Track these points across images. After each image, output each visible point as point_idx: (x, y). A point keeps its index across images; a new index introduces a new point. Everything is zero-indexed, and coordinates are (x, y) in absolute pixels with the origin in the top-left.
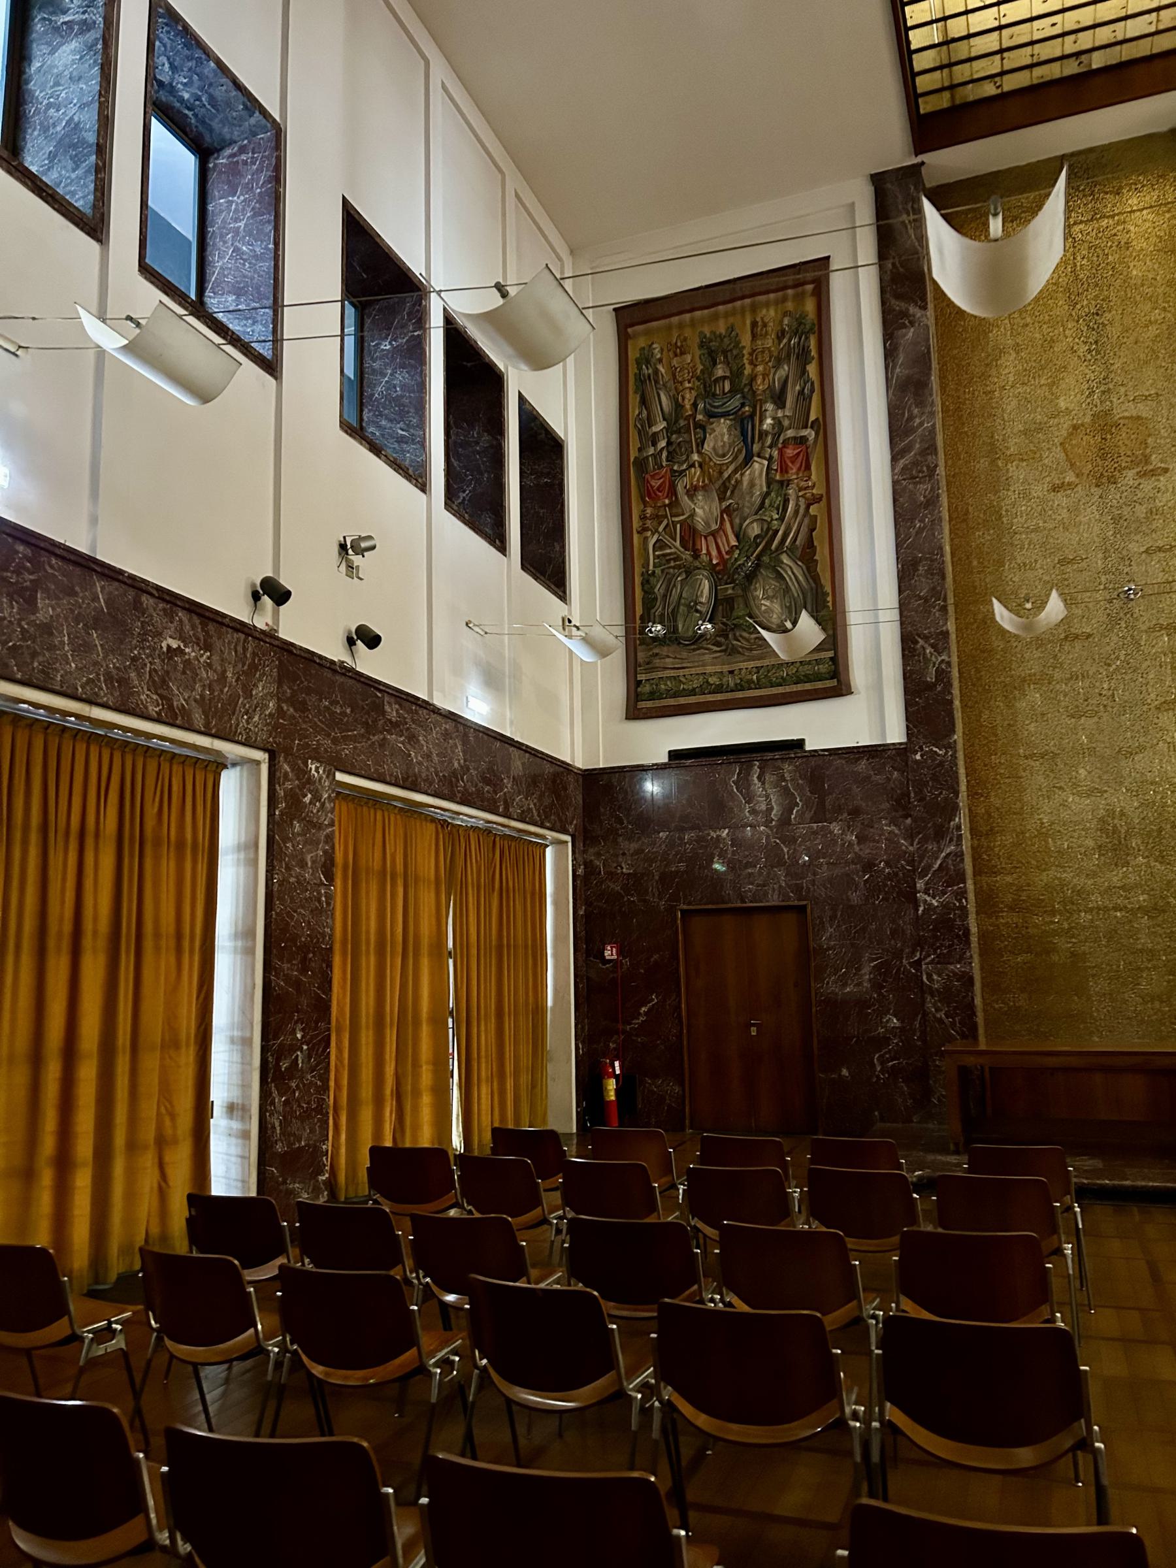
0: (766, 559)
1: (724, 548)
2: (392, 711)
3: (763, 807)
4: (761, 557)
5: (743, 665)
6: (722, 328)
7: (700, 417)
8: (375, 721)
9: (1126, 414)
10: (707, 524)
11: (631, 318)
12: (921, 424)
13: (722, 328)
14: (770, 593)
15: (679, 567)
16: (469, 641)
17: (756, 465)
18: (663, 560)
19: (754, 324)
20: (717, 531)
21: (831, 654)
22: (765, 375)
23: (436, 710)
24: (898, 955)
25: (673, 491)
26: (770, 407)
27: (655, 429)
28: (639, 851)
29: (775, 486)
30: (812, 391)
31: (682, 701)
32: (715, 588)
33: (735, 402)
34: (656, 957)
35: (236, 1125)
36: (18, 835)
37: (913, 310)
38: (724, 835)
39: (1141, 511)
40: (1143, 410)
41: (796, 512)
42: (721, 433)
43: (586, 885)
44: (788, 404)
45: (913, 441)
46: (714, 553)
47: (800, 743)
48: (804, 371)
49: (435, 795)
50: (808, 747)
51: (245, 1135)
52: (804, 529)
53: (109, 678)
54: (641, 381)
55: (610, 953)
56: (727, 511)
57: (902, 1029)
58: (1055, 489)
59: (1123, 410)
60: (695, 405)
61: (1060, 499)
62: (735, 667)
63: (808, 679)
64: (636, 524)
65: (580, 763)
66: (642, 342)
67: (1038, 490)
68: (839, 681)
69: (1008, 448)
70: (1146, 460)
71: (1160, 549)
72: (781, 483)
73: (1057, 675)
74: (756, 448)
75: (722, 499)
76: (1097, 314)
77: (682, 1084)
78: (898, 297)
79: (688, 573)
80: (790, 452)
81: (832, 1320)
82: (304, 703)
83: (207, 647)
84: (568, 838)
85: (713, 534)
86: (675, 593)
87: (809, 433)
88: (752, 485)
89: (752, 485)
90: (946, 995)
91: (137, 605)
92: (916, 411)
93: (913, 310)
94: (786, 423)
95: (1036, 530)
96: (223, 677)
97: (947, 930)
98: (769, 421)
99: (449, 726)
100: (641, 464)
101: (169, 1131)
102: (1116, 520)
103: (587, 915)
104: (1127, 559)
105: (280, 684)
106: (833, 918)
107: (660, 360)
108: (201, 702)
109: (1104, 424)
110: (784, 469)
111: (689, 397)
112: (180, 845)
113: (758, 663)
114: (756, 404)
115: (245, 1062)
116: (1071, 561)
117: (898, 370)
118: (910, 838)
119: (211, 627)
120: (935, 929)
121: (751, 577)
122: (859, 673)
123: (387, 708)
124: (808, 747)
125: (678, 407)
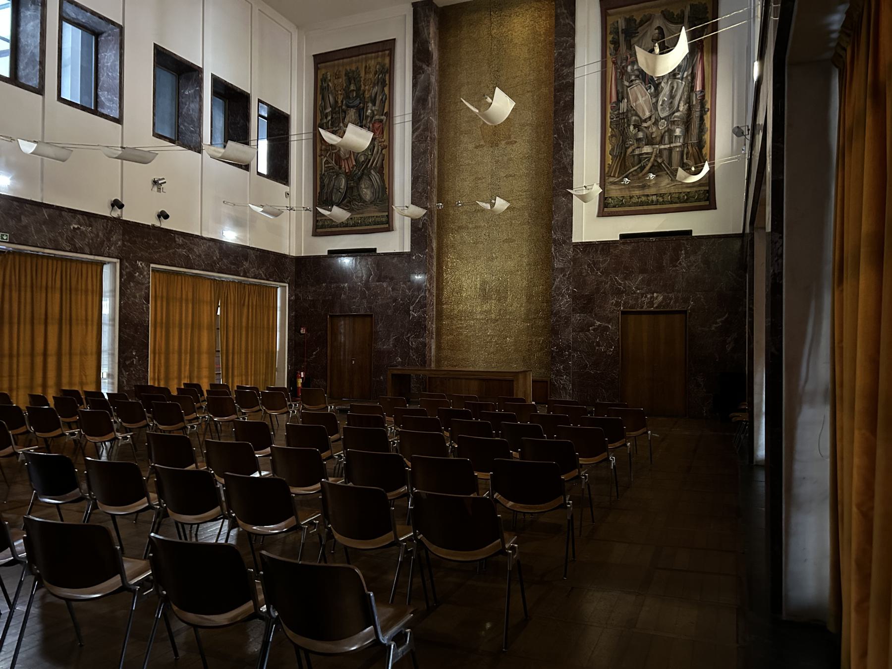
1: (351, 166)
2: (180, 241)
6: (354, 68)
11: (320, 60)
16: (226, 210)
18: (329, 169)
22: (369, 91)
26: (370, 105)
28: (315, 291)
31: (333, 229)
32: (347, 182)
33: (357, 102)
35: (110, 380)
36: (23, 289)
37: (424, 66)
39: (506, 158)
48: (383, 90)
49: (203, 270)
51: (113, 384)
53: (50, 240)
54: (322, 89)
55: (303, 331)
58: (476, 147)
65: (293, 254)
66: (323, 71)
67: (471, 146)
70: (510, 138)
71: (511, 176)
73: (470, 226)
78: (419, 60)
79: (337, 175)
81: (324, 455)
83: (91, 226)
85: (347, 159)
91: (61, 216)
93: (424, 66)
95: (469, 164)
96: (97, 236)
97: (419, 326)
99: (211, 244)
101: (84, 381)
102: (497, 162)
103: (296, 316)
105: (123, 235)
108: (88, 245)
111: (340, 98)
112: (87, 291)
114: (365, 103)
115: (113, 361)
116: (480, 179)
119: (92, 219)
121: (360, 179)
122: (397, 222)
125: (336, 102)
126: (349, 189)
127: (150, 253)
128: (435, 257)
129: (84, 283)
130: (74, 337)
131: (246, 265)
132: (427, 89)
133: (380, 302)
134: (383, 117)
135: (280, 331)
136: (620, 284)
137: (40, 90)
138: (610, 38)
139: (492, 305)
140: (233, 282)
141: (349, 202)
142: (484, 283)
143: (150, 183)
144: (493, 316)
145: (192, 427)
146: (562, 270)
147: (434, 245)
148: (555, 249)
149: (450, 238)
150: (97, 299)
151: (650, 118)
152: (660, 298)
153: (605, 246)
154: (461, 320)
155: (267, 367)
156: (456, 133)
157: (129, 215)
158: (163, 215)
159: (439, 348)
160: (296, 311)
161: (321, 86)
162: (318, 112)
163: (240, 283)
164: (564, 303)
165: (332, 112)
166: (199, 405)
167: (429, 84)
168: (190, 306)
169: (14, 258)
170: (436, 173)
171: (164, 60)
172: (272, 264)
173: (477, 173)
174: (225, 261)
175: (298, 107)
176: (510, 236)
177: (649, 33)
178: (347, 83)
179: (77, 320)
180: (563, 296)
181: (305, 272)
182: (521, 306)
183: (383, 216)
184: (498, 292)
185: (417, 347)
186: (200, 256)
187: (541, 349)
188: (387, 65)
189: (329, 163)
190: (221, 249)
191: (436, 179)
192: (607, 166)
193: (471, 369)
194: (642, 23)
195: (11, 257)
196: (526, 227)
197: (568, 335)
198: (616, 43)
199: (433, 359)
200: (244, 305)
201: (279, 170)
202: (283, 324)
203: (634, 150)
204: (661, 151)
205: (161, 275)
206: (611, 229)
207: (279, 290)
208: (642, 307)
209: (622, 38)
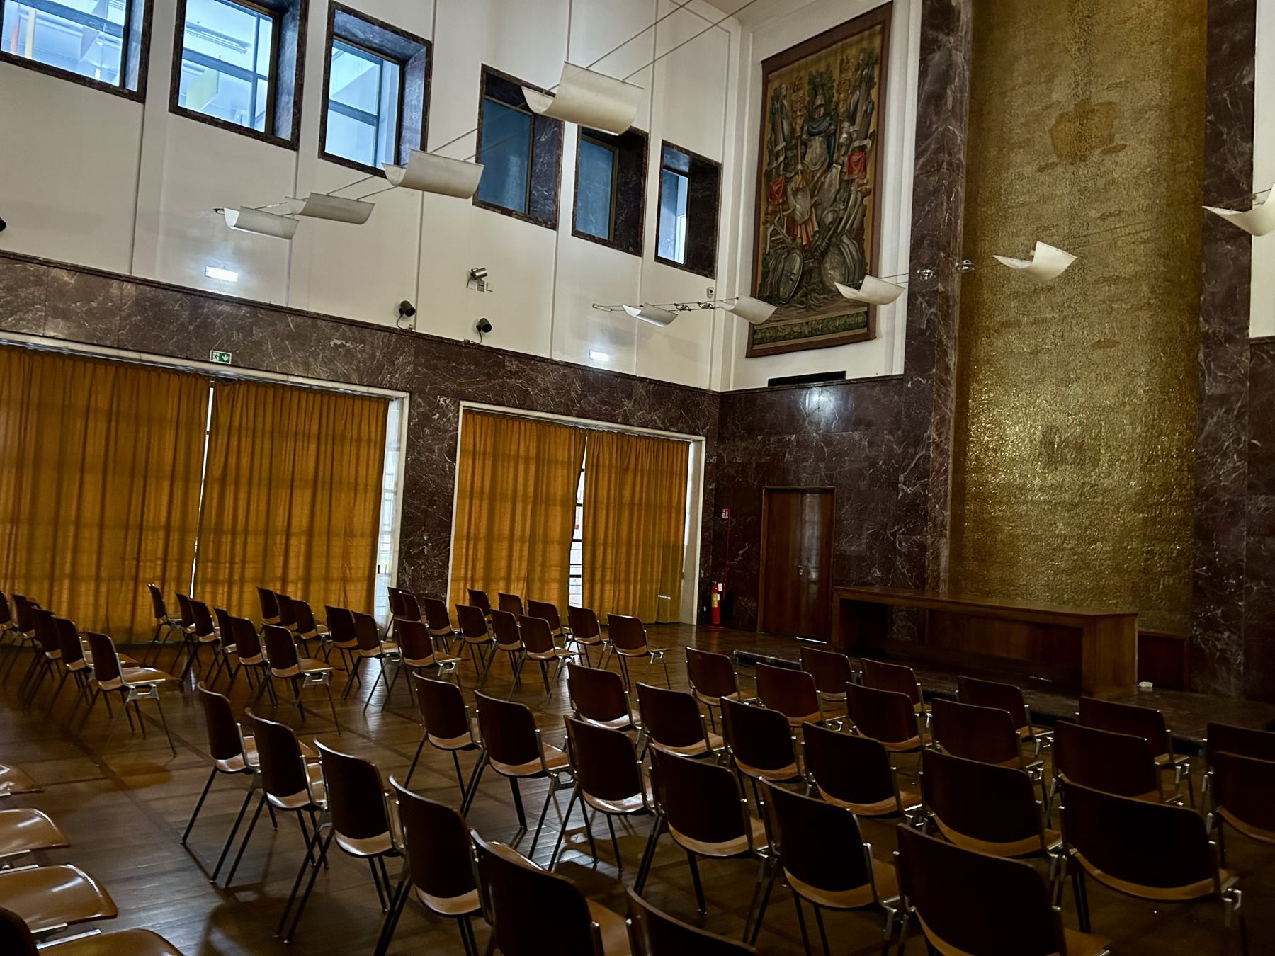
0: (834, 240)
1: (811, 233)
4: (830, 237)
5: (814, 318)
6: (822, 68)
8: (496, 372)
13: (822, 68)
15: (783, 248)
16: (596, 318)
19: (842, 61)
23: (556, 363)
24: (884, 526)
25: (785, 193)
26: (846, 124)
27: (779, 148)
28: (746, 448)
29: (844, 185)
32: (803, 261)
33: (826, 124)
37: (942, 37)
40: (1113, 96)
42: (817, 146)
43: (713, 472)
46: (804, 236)
47: (842, 374)
48: (869, 94)
50: (848, 377)
52: (859, 215)
54: (773, 113)
55: (725, 515)
56: (814, 205)
57: (882, 578)
58: (1041, 169)
59: (1101, 96)
61: (1044, 178)
62: (809, 319)
63: (851, 327)
65: (717, 388)
66: (776, 84)
67: (1029, 170)
70: (1111, 140)
71: (1111, 215)
74: (835, 156)
75: (812, 197)
77: (757, 602)
79: (789, 252)
80: (855, 158)
82: (435, 365)
83: (363, 342)
84: (704, 439)
85: (805, 223)
86: (780, 267)
87: (868, 142)
88: (830, 185)
89: (830, 185)
90: (909, 557)
92: (934, 119)
93: (942, 37)
94: (855, 136)
95: (1024, 204)
96: (373, 356)
97: (915, 513)
98: (844, 136)
100: (768, 175)
102: (1082, 192)
103: (717, 489)
105: (416, 356)
106: (849, 499)
109: (1084, 111)
110: (850, 172)
111: (800, 122)
112: (359, 440)
114: (836, 121)
116: (1046, 228)
118: (899, 444)
120: (908, 510)
123: (508, 364)
124: (848, 377)
125: (793, 130)
126: (806, 273)
127: (460, 385)
128: (954, 382)
129: (355, 427)
130: (333, 514)
131: (629, 405)
132: (945, 78)
133: (847, 466)
134: (868, 142)
135: (691, 513)
137: (293, 145)
139: (1066, 475)
140: (609, 432)
141: (805, 295)
142: (1049, 430)
143: (465, 278)
144: (1068, 497)
145: (658, 654)
146: (1223, 400)
147: (953, 360)
148: (1207, 355)
149: (984, 347)
150: (373, 454)
154: (1000, 502)
155: (664, 571)
156: (1000, 150)
157: (424, 325)
158: (407, 310)
159: (956, 555)
160: (718, 482)
161: (772, 108)
162: (766, 150)
163: (621, 434)
164: (1229, 470)
165: (786, 149)
166: (558, 632)
167: (951, 65)
168: (532, 468)
169: (10, 357)
170: (960, 227)
171: (500, 90)
172: (678, 404)
173: (1040, 218)
174: (592, 399)
175: (733, 147)
176: (1108, 336)
178: (813, 99)
179: (341, 483)
181: (741, 421)
182: (1129, 478)
183: (858, 315)
184: (1079, 448)
185: (910, 552)
186: (546, 390)
187: (1176, 570)
188: (878, 50)
189: (778, 233)
190: (584, 380)
191: (960, 239)
193: (996, 602)
195: (243, 388)
196: (1145, 315)
197: (1239, 542)
199: (944, 575)
200: (627, 469)
201: (701, 258)
202: (695, 503)
205: (485, 420)
207: (692, 447)
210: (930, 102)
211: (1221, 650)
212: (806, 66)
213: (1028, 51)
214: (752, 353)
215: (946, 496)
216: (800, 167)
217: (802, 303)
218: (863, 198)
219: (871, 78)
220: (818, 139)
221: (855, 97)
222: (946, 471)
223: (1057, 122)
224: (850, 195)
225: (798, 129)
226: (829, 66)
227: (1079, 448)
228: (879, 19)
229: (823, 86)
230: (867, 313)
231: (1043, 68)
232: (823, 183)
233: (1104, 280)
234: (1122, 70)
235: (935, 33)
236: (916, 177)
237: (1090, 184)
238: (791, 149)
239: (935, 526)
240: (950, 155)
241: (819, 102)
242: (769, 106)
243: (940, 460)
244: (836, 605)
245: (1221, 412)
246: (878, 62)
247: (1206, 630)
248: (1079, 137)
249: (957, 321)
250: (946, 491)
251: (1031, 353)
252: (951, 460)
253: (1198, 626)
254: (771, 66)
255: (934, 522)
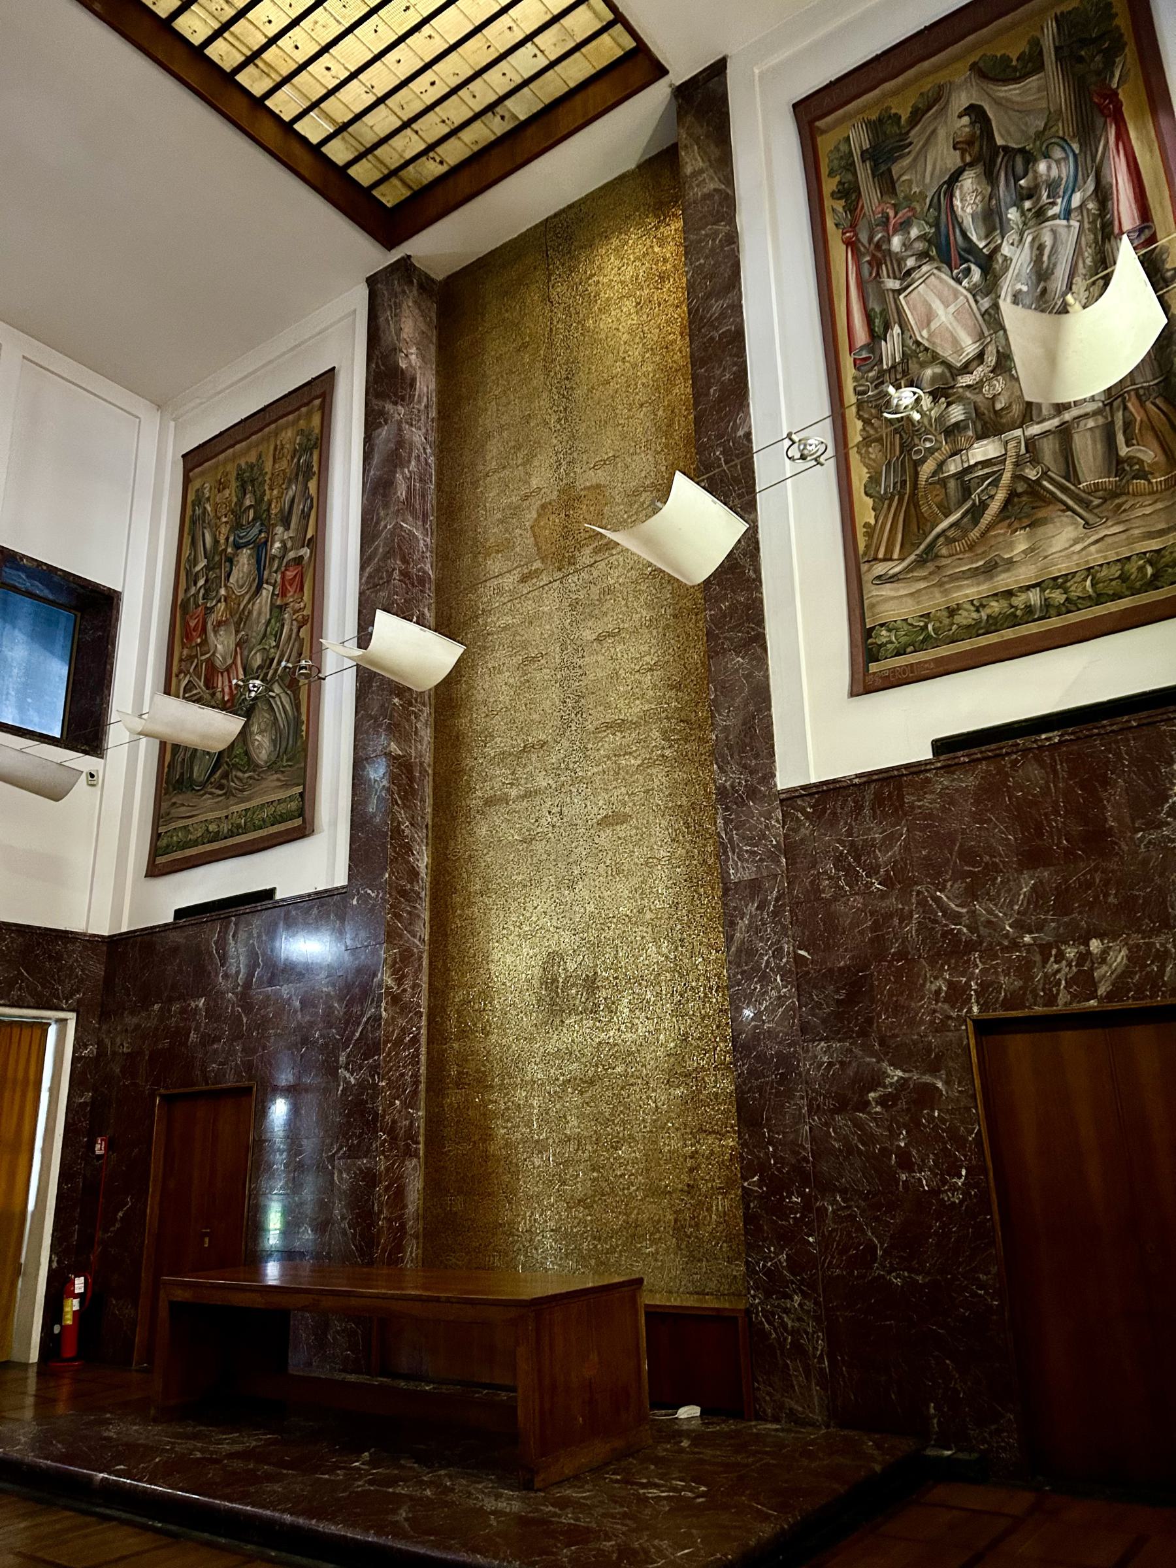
3: (234, 970)
5: (235, 809)
6: (252, 458)
7: (229, 550)
9: (588, 484)
10: (224, 659)
12: (386, 526)
13: (252, 458)
14: (263, 726)
17: (264, 592)
19: (276, 446)
20: (230, 666)
21: (300, 789)
25: (204, 630)
26: (279, 530)
27: (198, 568)
29: (276, 612)
30: (311, 507)
33: (255, 531)
34: (136, 1150)
37: (389, 407)
38: (201, 1004)
39: (595, 590)
40: (600, 476)
41: (290, 637)
44: (293, 525)
45: (378, 545)
46: (227, 690)
47: (270, 893)
48: (307, 488)
50: (279, 896)
54: (193, 522)
55: (99, 1148)
58: (524, 579)
59: (587, 478)
60: (227, 539)
64: (175, 670)
65: (103, 928)
67: (509, 581)
68: (304, 820)
69: (487, 540)
72: (280, 607)
75: (237, 632)
76: (567, 378)
80: (290, 574)
84: (71, 1016)
85: (228, 670)
88: (260, 614)
92: (382, 513)
93: (389, 407)
94: (289, 544)
98: (277, 545)
104: (580, 650)
107: (208, 499)
109: (569, 499)
110: (284, 594)
111: (224, 530)
113: (247, 805)
114: (267, 527)
116: (534, 659)
117: (372, 472)
132: (396, 458)
134: (305, 552)
136: (956, 918)
138: (830, 185)
141: (225, 775)
142: (554, 958)
146: (754, 887)
147: (423, 861)
151: (980, 357)
152: (1119, 957)
153: (887, 788)
159: (435, 1186)
160: (95, 1090)
167: (400, 443)
177: (942, 133)
180: (764, 979)
188: (317, 431)
192: (860, 531)
194: (917, 116)
196: (659, 775)
198: (849, 193)
203: (941, 465)
204: (1031, 443)
206: (902, 728)
207: (52, 1031)
208: (1051, 1000)
209: (863, 173)
210: (377, 491)
211: (795, 1332)
212: (234, 458)
213: (501, 426)
214: (155, 870)
215: (416, 1083)
216: (223, 592)
217: (221, 787)
218: (299, 628)
219: (309, 466)
220: (246, 552)
221: (291, 493)
222: (415, 1040)
223: (539, 515)
224: (283, 625)
225: (222, 541)
226: (260, 456)
227: (591, 985)
228: (318, 392)
229: (253, 481)
230: (301, 795)
231: (519, 447)
232: (250, 612)
233: (608, 726)
234: (609, 442)
235: (380, 403)
236: (361, 594)
237: (582, 595)
238: (213, 569)
239: (393, 1139)
240: (405, 561)
241: (248, 503)
242: (189, 512)
243: (402, 1022)
244: (163, 1313)
245: (752, 907)
246: (318, 444)
247: (768, 1295)
248: (566, 533)
249: (429, 801)
250: (416, 1076)
251: (524, 841)
252: (424, 1023)
253: (757, 1288)
254: (194, 460)
255: (392, 1131)
